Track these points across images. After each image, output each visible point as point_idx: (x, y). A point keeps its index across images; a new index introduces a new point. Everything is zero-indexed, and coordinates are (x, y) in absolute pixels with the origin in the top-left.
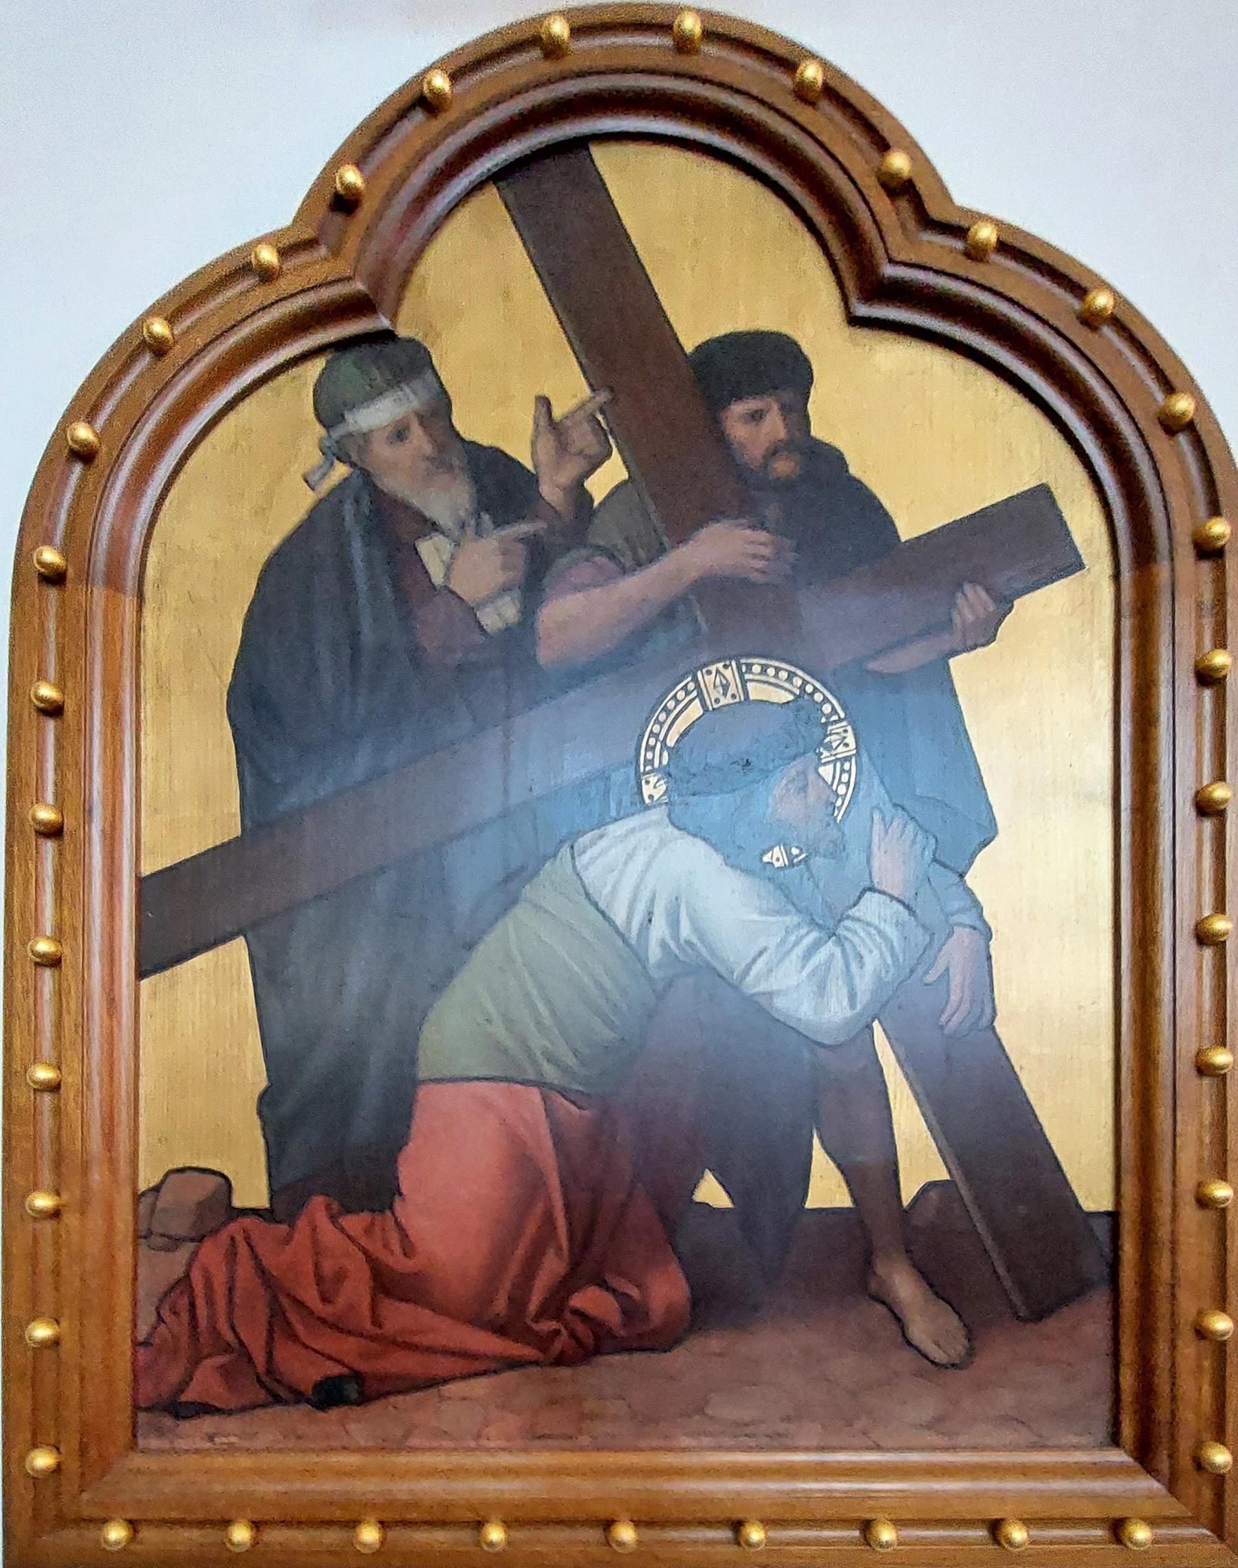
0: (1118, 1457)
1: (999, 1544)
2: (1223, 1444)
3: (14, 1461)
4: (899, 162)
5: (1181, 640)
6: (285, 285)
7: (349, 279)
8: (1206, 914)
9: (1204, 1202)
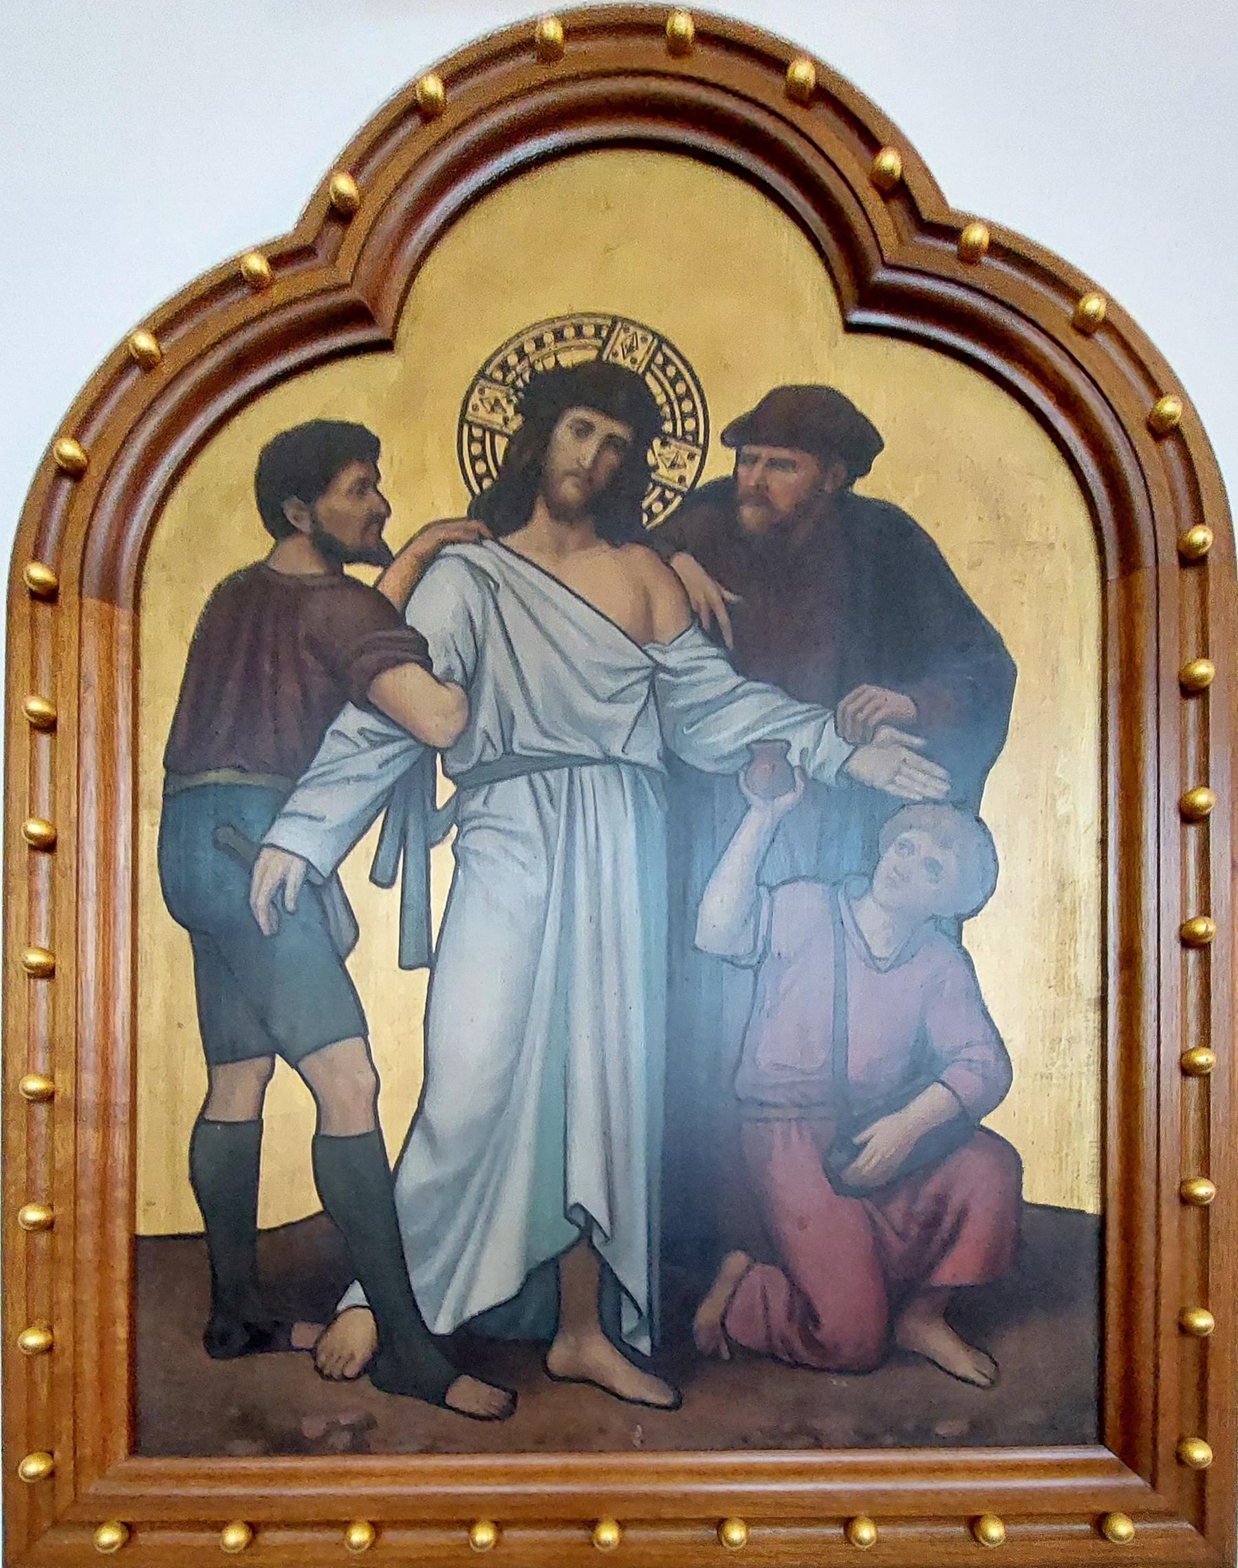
0: (1106, 1454)
1: (977, 1541)
2: (1205, 1441)
3: (11, 1471)
4: (889, 160)
5: (1170, 651)
6: (277, 294)
7: (347, 286)
8: (1191, 916)
9: (1186, 1200)
